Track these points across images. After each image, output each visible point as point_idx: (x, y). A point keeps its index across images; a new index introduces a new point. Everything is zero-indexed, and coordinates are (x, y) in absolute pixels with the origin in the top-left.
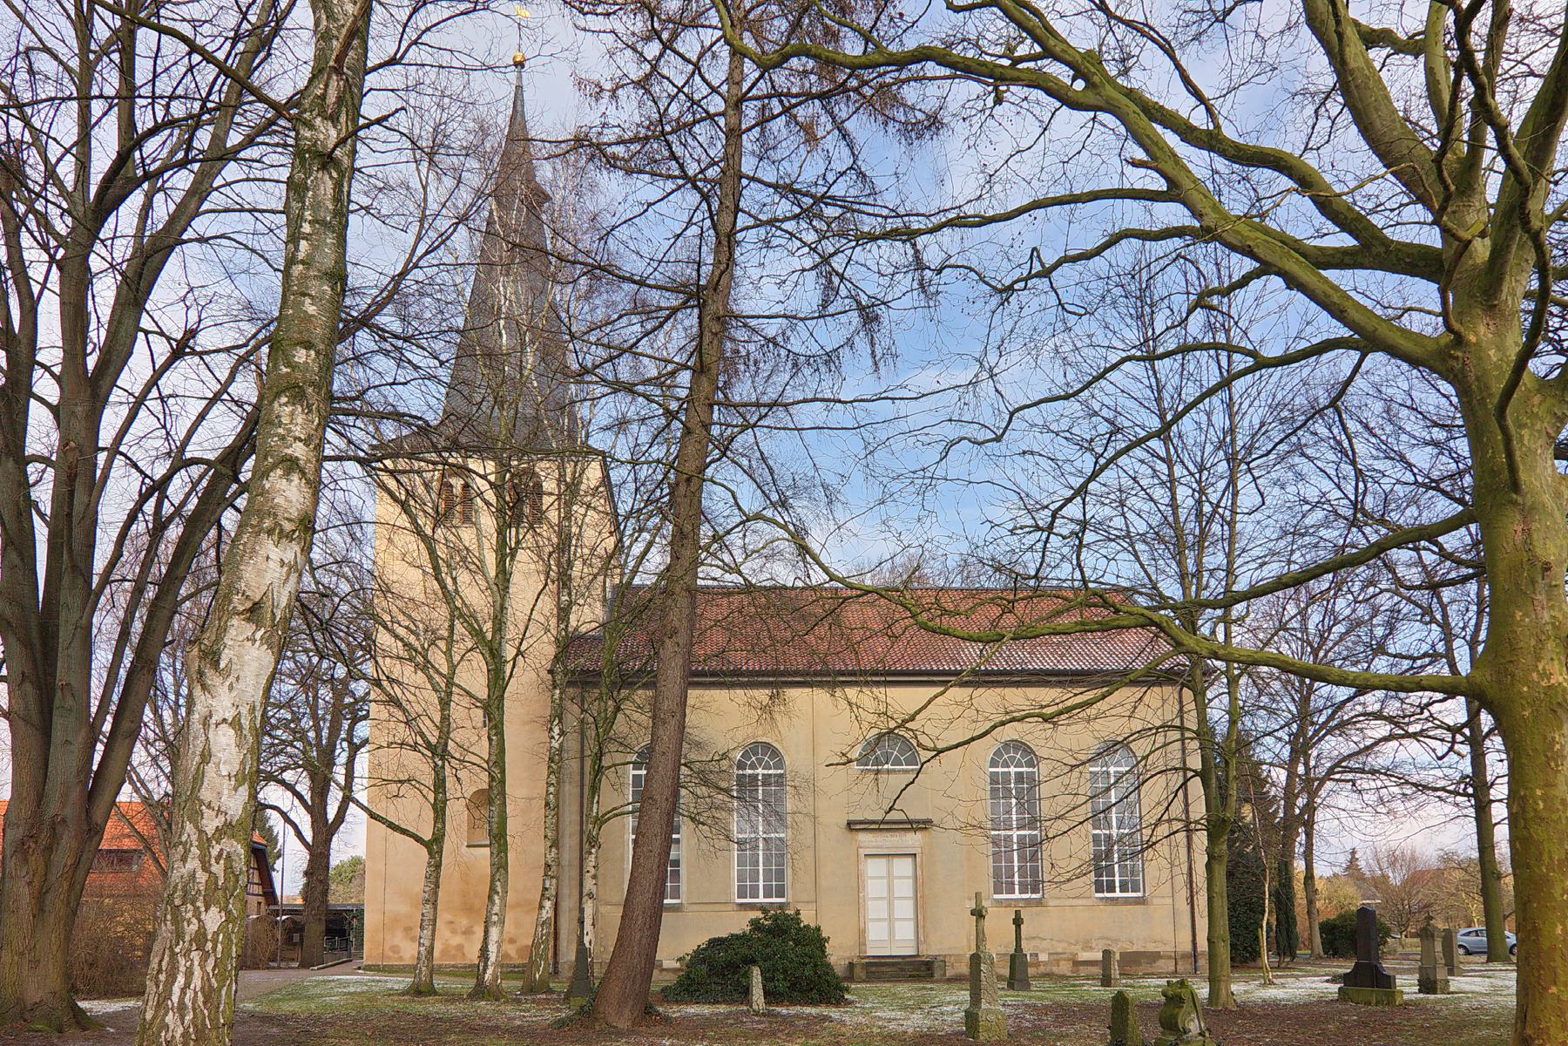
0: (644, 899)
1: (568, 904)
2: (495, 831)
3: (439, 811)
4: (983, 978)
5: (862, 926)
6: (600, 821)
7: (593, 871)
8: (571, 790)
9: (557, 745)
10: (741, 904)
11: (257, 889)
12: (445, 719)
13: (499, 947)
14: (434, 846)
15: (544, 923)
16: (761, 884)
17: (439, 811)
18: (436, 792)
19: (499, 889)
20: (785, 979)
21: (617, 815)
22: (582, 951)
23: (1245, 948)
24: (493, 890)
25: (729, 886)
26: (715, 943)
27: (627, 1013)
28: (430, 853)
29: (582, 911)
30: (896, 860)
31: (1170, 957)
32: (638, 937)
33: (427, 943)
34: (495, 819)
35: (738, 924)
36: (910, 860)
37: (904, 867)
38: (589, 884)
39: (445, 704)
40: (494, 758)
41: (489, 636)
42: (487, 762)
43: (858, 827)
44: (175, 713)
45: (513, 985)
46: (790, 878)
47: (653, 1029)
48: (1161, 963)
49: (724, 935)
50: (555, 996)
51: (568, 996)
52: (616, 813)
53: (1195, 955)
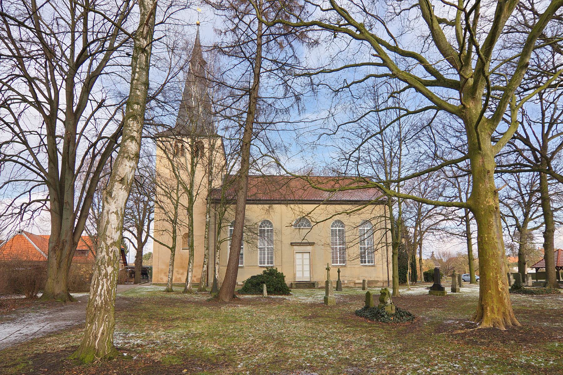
0: (233, 265)
3: (174, 239)
6: (220, 242)
7: (218, 257)
10: (260, 266)
12: (176, 213)
14: (173, 249)
17: (174, 239)
22: (215, 280)
24: (189, 262)
27: (228, 297)
29: (215, 268)
33: (171, 277)
35: (260, 272)
36: (308, 254)
37: (307, 256)
39: (176, 208)
40: (190, 224)
41: (189, 189)
48: (379, 283)
52: (225, 240)
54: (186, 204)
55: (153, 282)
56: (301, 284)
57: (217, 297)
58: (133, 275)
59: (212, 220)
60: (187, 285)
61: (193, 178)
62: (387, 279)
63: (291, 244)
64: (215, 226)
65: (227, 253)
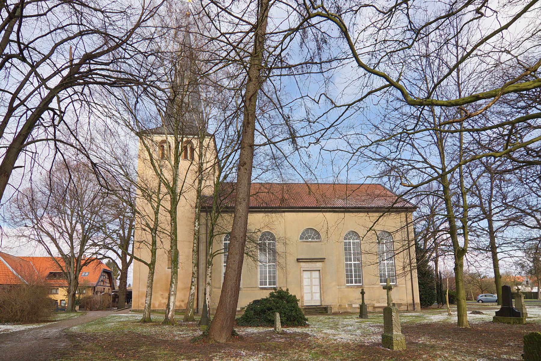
0: (231, 283)
1: (201, 288)
2: (173, 259)
3: (154, 253)
4: (393, 320)
5: (302, 295)
6: (212, 256)
7: (210, 274)
8: (202, 247)
9: (197, 229)
10: (261, 288)
11: (108, 285)
12: (156, 219)
13: (174, 304)
14: (152, 266)
15: (192, 295)
16: (268, 280)
17: (154, 253)
18: (153, 246)
19: (174, 282)
20: (284, 317)
21: (218, 254)
22: (205, 305)
23: (429, 302)
24: (172, 282)
25: (257, 281)
26: (256, 302)
27: (224, 335)
28: (150, 269)
29: (205, 289)
30: (313, 272)
31: (405, 305)
32: (229, 301)
33: (148, 303)
34: (173, 255)
35: (265, 295)
36: (318, 272)
37: (316, 274)
38: (208, 279)
39: (156, 213)
40: (173, 231)
41: (171, 186)
42: (170, 233)
43: (300, 261)
44: (71, 223)
45: (180, 317)
46: (277, 278)
47: (236, 343)
48: (402, 307)
49: (259, 299)
50: (196, 322)
51: (200, 323)
52: (218, 253)
53: (414, 304)
54: (168, 206)
55: (133, 308)
56: (311, 309)
57: (206, 336)
58: (117, 300)
59: (203, 231)
60: (168, 313)
61: (176, 172)
62: (412, 302)
63: (297, 259)
64: (207, 236)
65: (220, 272)
